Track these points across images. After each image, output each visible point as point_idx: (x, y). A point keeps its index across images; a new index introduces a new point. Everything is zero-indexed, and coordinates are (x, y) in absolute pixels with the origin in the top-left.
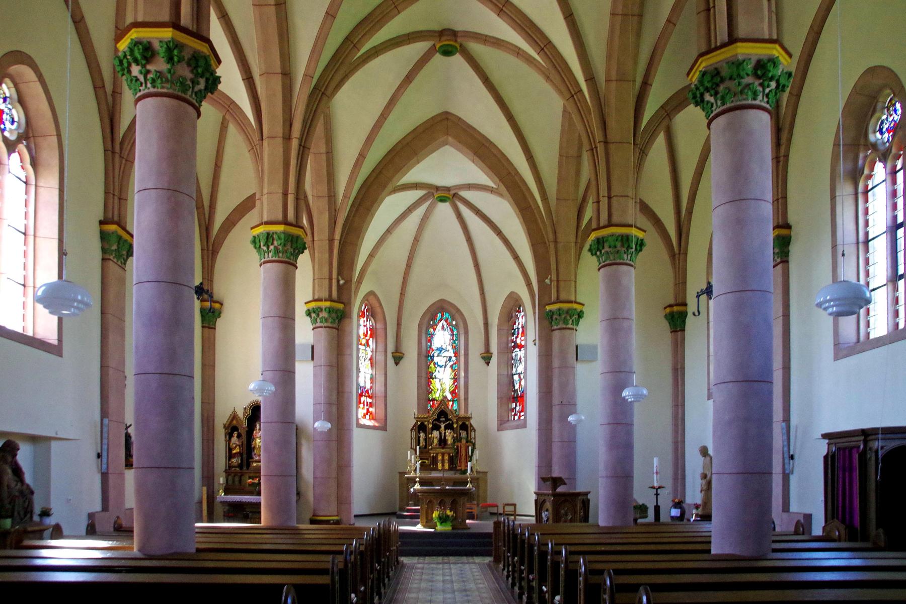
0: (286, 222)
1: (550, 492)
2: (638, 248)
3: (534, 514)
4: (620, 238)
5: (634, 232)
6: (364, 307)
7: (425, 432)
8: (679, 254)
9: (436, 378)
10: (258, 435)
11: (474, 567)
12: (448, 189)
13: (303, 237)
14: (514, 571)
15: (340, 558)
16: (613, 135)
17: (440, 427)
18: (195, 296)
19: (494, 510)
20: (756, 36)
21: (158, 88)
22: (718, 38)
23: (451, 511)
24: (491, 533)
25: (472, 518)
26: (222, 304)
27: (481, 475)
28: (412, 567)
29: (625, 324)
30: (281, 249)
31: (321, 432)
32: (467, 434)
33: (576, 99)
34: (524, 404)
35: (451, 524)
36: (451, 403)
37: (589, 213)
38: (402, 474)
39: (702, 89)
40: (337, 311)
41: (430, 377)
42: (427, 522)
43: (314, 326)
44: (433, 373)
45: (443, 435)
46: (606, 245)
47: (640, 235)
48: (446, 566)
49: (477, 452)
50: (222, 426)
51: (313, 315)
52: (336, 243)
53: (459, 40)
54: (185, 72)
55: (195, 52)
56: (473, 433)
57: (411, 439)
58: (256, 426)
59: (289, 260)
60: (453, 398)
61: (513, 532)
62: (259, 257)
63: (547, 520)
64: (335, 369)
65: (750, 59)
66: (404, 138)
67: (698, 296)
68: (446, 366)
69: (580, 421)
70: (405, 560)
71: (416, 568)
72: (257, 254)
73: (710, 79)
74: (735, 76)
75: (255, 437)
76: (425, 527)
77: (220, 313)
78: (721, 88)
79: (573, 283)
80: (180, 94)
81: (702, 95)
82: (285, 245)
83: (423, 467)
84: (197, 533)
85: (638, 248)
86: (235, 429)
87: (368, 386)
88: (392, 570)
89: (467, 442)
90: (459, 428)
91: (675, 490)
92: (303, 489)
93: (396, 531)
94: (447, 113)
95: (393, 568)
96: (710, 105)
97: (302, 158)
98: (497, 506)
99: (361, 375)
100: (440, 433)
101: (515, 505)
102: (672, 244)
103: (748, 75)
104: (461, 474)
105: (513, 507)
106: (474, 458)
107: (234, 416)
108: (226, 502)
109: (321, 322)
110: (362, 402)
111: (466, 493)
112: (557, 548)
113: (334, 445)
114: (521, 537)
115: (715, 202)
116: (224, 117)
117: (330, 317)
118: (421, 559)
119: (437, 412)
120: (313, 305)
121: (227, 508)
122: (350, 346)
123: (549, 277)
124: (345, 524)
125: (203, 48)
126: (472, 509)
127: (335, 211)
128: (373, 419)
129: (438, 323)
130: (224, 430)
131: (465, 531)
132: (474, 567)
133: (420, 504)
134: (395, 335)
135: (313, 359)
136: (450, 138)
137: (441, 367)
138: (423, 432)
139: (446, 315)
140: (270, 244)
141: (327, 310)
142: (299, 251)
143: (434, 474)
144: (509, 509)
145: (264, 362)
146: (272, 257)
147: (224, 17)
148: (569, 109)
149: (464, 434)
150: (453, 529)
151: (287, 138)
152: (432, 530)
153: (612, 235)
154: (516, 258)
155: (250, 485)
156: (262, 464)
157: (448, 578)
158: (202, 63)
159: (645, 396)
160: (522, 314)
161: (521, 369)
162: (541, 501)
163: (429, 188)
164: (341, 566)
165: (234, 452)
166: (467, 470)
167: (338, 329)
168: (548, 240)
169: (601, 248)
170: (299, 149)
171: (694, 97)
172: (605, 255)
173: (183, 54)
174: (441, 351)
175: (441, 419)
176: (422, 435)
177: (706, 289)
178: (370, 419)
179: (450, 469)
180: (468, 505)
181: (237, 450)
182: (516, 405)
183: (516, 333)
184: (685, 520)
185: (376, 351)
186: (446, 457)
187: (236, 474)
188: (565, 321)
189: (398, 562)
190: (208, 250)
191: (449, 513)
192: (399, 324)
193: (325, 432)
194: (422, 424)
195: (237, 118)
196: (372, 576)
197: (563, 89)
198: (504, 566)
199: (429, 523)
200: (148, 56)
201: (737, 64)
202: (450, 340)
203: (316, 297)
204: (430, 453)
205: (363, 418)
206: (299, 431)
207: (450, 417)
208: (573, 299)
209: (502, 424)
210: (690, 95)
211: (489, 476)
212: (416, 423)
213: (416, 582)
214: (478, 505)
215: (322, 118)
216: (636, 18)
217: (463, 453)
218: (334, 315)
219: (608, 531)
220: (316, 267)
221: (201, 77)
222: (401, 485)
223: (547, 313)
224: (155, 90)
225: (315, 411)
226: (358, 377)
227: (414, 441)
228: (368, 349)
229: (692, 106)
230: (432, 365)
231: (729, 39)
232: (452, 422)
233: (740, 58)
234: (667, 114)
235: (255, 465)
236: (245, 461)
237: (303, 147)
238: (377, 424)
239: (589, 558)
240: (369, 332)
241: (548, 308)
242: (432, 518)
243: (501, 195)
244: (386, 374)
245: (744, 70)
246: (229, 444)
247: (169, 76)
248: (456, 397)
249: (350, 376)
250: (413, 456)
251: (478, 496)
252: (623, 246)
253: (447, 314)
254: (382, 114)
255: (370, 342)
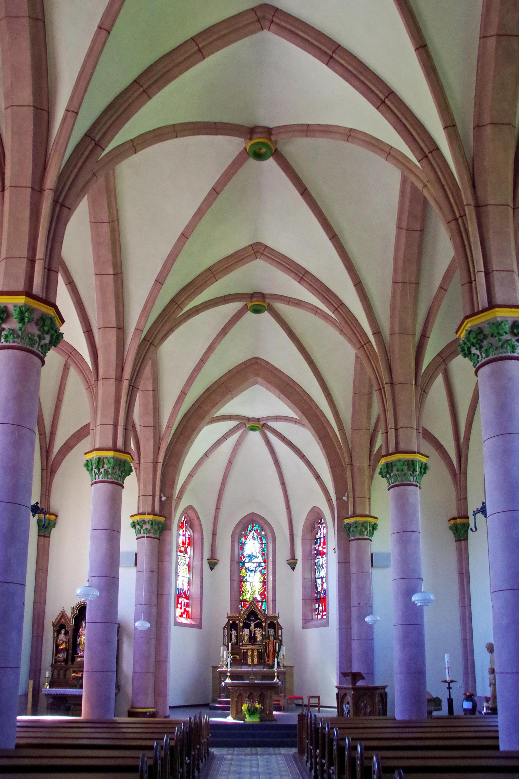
0: (115, 449)
1: (351, 686)
2: (423, 471)
3: (336, 706)
4: (406, 463)
5: (418, 457)
6: (183, 519)
7: (236, 630)
8: (460, 474)
9: (247, 581)
10: (84, 632)
11: (279, 759)
12: (258, 420)
13: (130, 461)
14: (316, 764)
15: (151, 754)
16: (398, 377)
17: (251, 626)
18: (31, 514)
19: (300, 702)
20: (511, 303)
21: (10, 342)
22: (480, 303)
23: (259, 704)
24: (296, 725)
25: (279, 709)
26: (57, 516)
27: (287, 670)
28: (221, 758)
29: (414, 536)
30: (110, 472)
31: (141, 631)
32: (275, 632)
33: (366, 349)
34: (327, 606)
35: (259, 716)
36: (260, 604)
37: (379, 442)
38: (215, 668)
39: (469, 344)
40: (158, 523)
41: (241, 580)
42: (236, 714)
43: (138, 536)
44: (244, 577)
45: (253, 633)
46: (395, 469)
47: (424, 460)
48: (254, 757)
49: (284, 648)
50: (52, 624)
51: (138, 527)
52: (160, 466)
53: (267, 301)
54: (34, 330)
55: (43, 314)
56: (280, 631)
57: (224, 636)
58: (82, 624)
59: (117, 481)
60: (263, 599)
61: (315, 726)
62: (91, 478)
63: (348, 713)
64: (156, 574)
65: (507, 321)
66: (220, 378)
67: (474, 515)
68: (255, 571)
69: (376, 621)
70: (214, 751)
71: (225, 760)
72: (89, 475)
73: (475, 336)
74: (495, 334)
75: (80, 634)
76: (235, 718)
77: (55, 524)
78: (485, 343)
79: (367, 500)
80: (28, 347)
81: (469, 349)
82: (113, 468)
83: (234, 662)
84: (18, 727)
85: (423, 471)
86: (62, 626)
87: (186, 588)
88: (202, 762)
89: (275, 639)
90: (267, 627)
91: (466, 683)
92: (122, 683)
93: (207, 723)
94: (257, 358)
95: (204, 759)
96: (476, 356)
97: (130, 397)
98: (302, 698)
99: (180, 579)
100: (250, 631)
101: (318, 697)
102: (454, 467)
103: (506, 333)
104: (269, 668)
105: (317, 699)
106: (282, 653)
107: (63, 615)
108: (51, 694)
109: (144, 533)
110: (180, 602)
111: (274, 687)
112: (353, 743)
113: (153, 641)
114: (322, 731)
115: (484, 436)
116: (66, 362)
117: (152, 528)
118: (231, 750)
119: (247, 612)
120: (138, 518)
121: (51, 700)
122: (170, 555)
123: (346, 495)
124: (161, 717)
125: (50, 311)
126: (279, 701)
127: (160, 438)
128: (189, 617)
129: (249, 533)
130: (52, 628)
131: (274, 723)
132: (279, 759)
133: (231, 696)
134: (211, 544)
135: (136, 565)
136: (259, 379)
137: (251, 571)
138: (234, 630)
139: (257, 526)
140: (100, 467)
141: (150, 522)
142: (126, 473)
143: (245, 669)
144: (314, 701)
145: (91, 569)
146: (102, 478)
147: (71, 284)
148: (359, 356)
149: (272, 632)
150: (260, 720)
151: (119, 379)
152: (242, 722)
153: (399, 460)
154: (318, 477)
155: (73, 679)
156: (85, 659)
157: (254, 770)
158: (48, 322)
159: (432, 600)
160: (324, 525)
161: (323, 573)
162: (342, 694)
163: (242, 419)
164: (151, 762)
165: (61, 647)
166: (274, 665)
167: (159, 540)
168: (345, 464)
169: (390, 471)
170: (129, 388)
171: (463, 350)
172: (394, 477)
173: (32, 316)
174: (251, 557)
175: (251, 618)
176: (234, 632)
177: (482, 508)
178: (186, 617)
179: (259, 664)
180: (275, 697)
181: (64, 646)
182: (319, 606)
183: (319, 542)
184: (477, 713)
185: (193, 558)
186: (256, 653)
187: (61, 668)
188: (361, 533)
189: (208, 753)
190: (47, 470)
191: (257, 705)
192: (214, 534)
193: (144, 631)
194: (234, 622)
195: (77, 362)
196: (181, 770)
197: (354, 340)
198: (307, 758)
199: (238, 714)
200: (4, 317)
201: (497, 325)
202: (260, 548)
203: (141, 511)
204: (241, 649)
205: (180, 616)
206: (120, 629)
207: (259, 616)
208: (367, 513)
209: (307, 622)
210: (459, 349)
211: (295, 669)
212: (228, 622)
213: (225, 773)
214: (285, 697)
215: (150, 362)
216: (413, 285)
217: (271, 648)
218: (156, 527)
219: (403, 725)
220: (142, 485)
221: (47, 334)
222: (214, 678)
223: (345, 525)
224: (8, 344)
225: (136, 612)
226: (176, 580)
227: (226, 638)
228: (186, 555)
229: (460, 357)
230: (243, 570)
231: (488, 305)
232: (261, 620)
233: (499, 320)
234: (444, 361)
235: (79, 659)
236: (70, 658)
237: (133, 387)
238: (193, 623)
239: (382, 753)
240: (187, 541)
241: (346, 521)
242: (242, 710)
243: (303, 425)
244: (202, 578)
245: (502, 329)
246: (57, 641)
247: (20, 333)
248: (265, 598)
249: (169, 580)
250: (225, 652)
251: (285, 689)
252: (409, 469)
253: (257, 526)
254: (201, 360)
255: (188, 550)
